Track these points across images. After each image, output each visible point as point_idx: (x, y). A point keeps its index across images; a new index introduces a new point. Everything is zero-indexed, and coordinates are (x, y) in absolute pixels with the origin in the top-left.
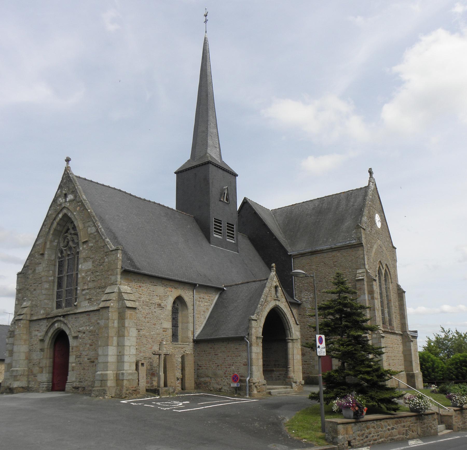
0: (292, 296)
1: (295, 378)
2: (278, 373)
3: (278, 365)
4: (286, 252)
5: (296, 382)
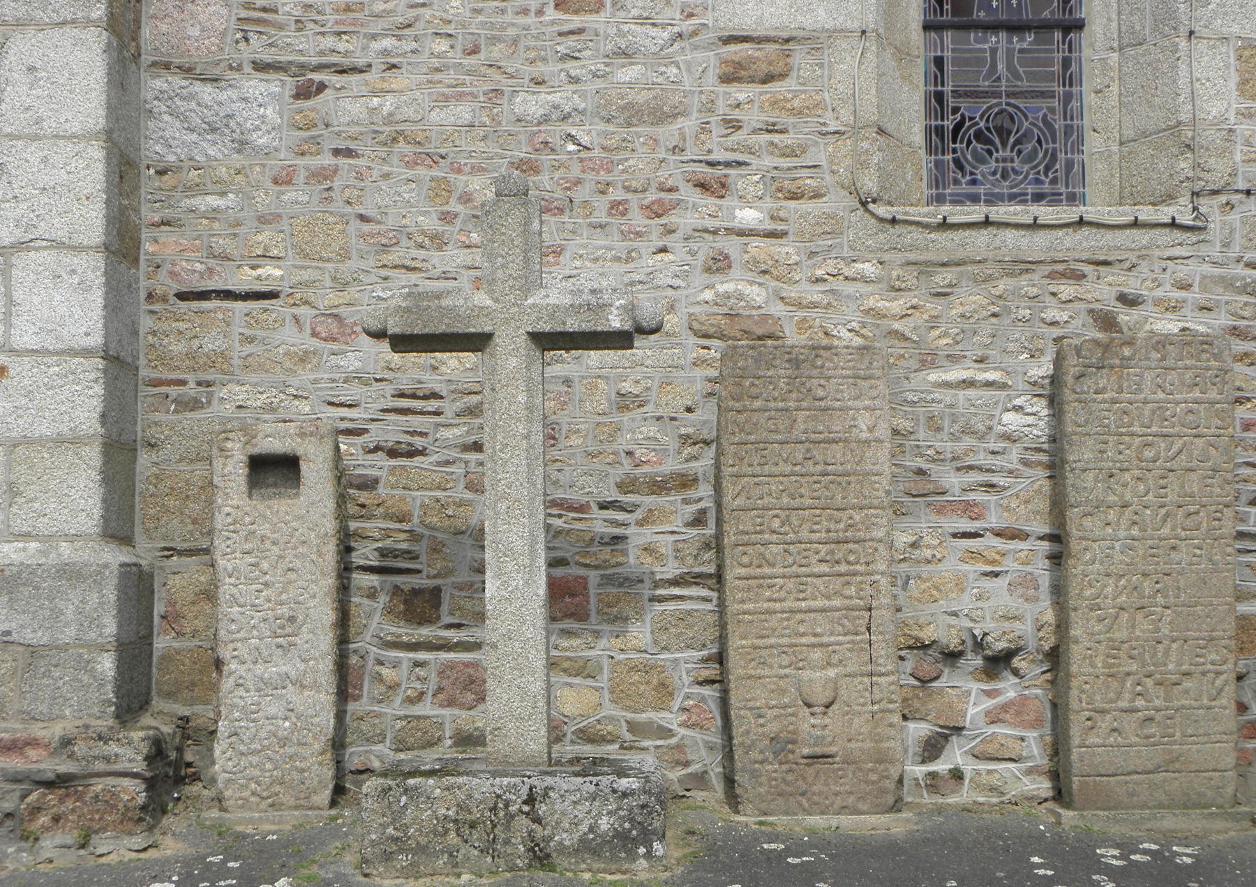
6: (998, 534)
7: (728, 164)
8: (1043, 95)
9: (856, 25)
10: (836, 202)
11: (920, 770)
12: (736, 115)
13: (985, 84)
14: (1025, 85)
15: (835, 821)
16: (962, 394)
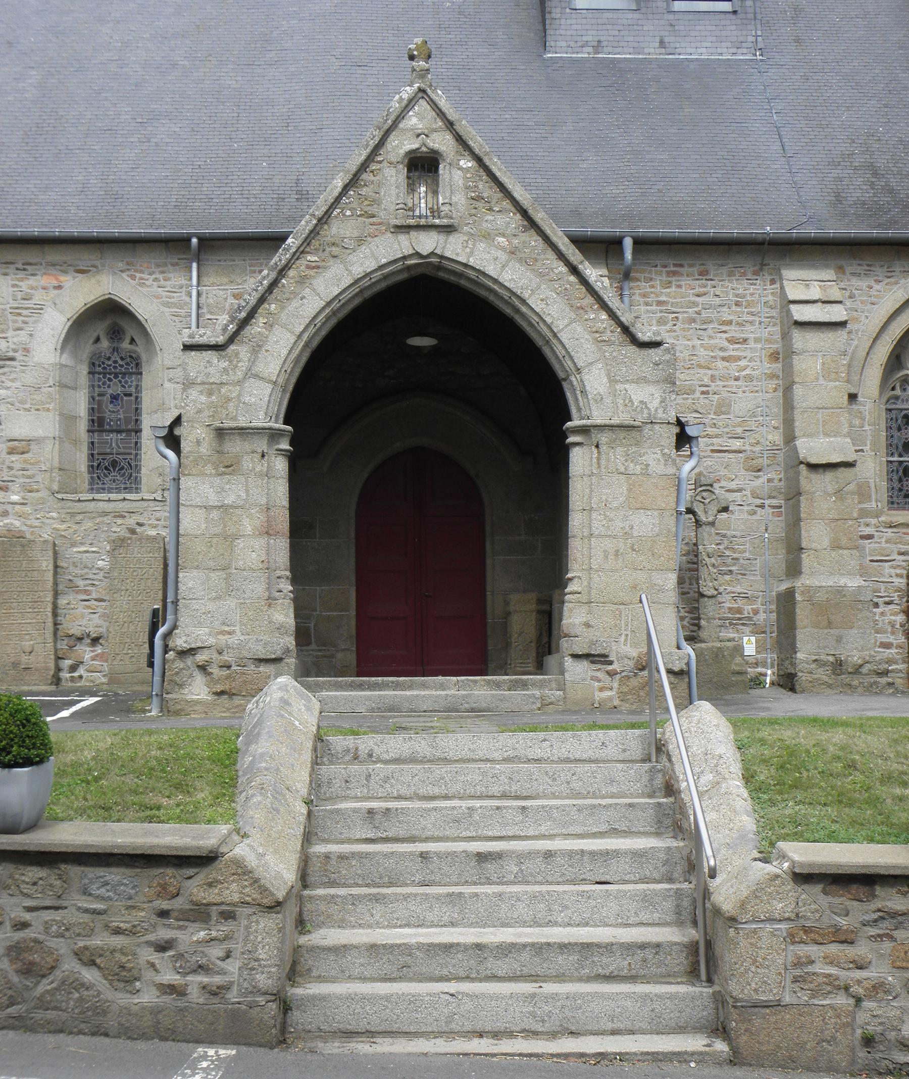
6: (96, 600)
7: (8, 481)
8: (128, 454)
9: (52, 436)
10: (44, 494)
11: (68, 675)
12: (12, 465)
13: (108, 450)
14: (122, 450)
15: (30, 688)
16: (85, 555)
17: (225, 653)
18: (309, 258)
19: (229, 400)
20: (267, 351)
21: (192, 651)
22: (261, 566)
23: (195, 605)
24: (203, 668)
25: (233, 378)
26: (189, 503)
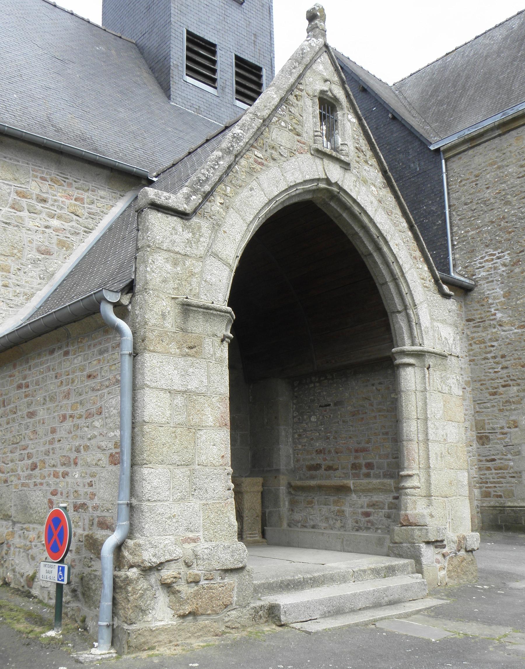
0: (444, 266)
1: (432, 524)
2: (364, 500)
3: (369, 466)
4: (423, 143)
5: (438, 544)
17: (195, 565)
18: (256, 153)
19: (193, 274)
20: (225, 232)
21: (158, 567)
22: (221, 461)
23: (160, 508)
24: (167, 586)
25: (195, 252)
26: (154, 385)
